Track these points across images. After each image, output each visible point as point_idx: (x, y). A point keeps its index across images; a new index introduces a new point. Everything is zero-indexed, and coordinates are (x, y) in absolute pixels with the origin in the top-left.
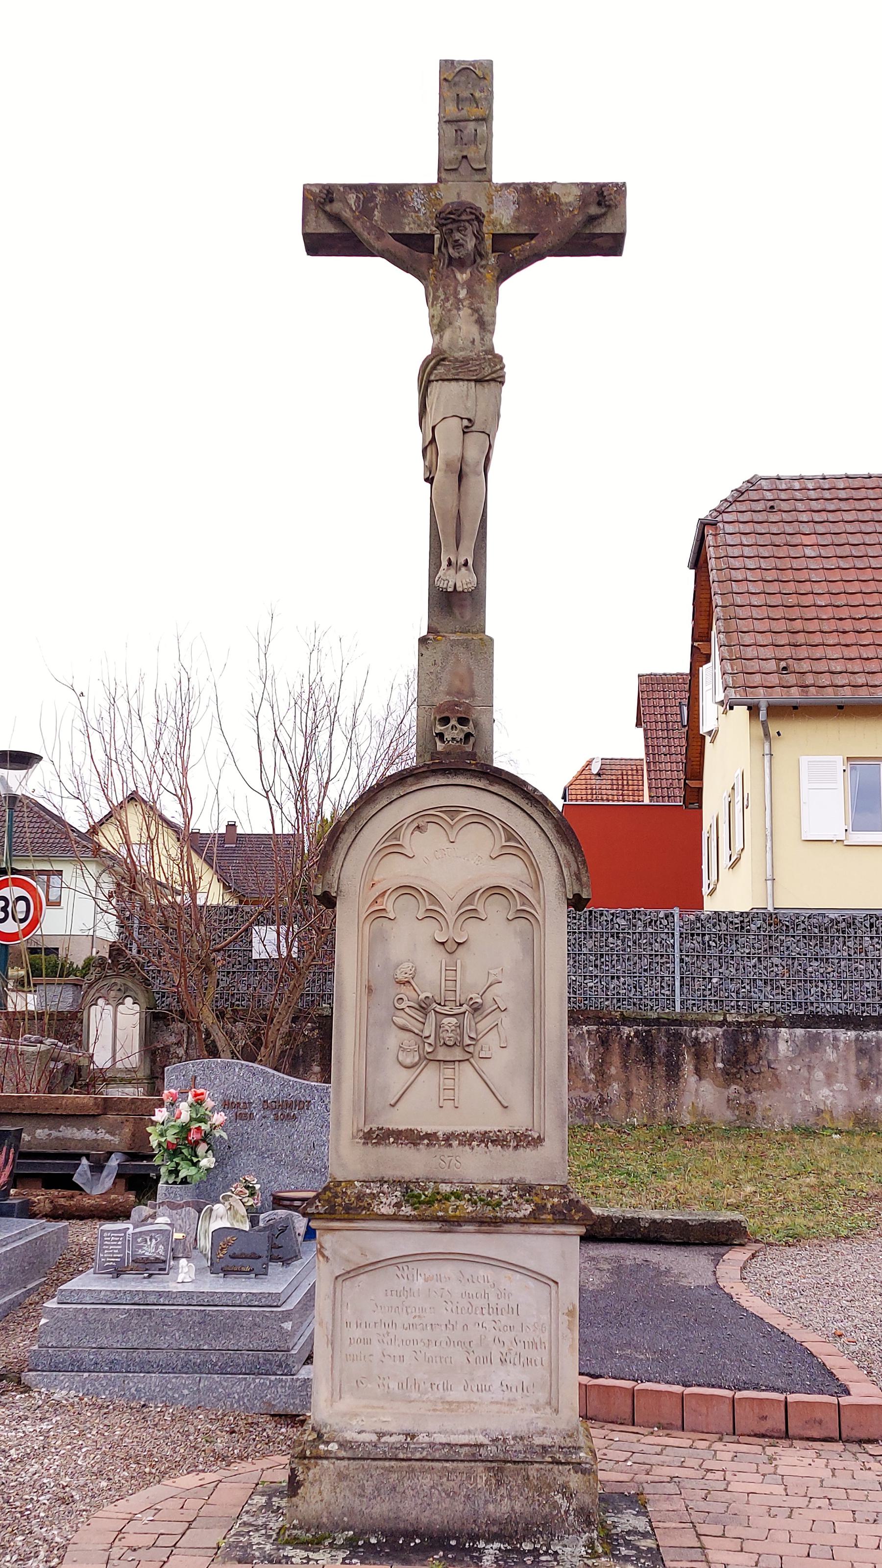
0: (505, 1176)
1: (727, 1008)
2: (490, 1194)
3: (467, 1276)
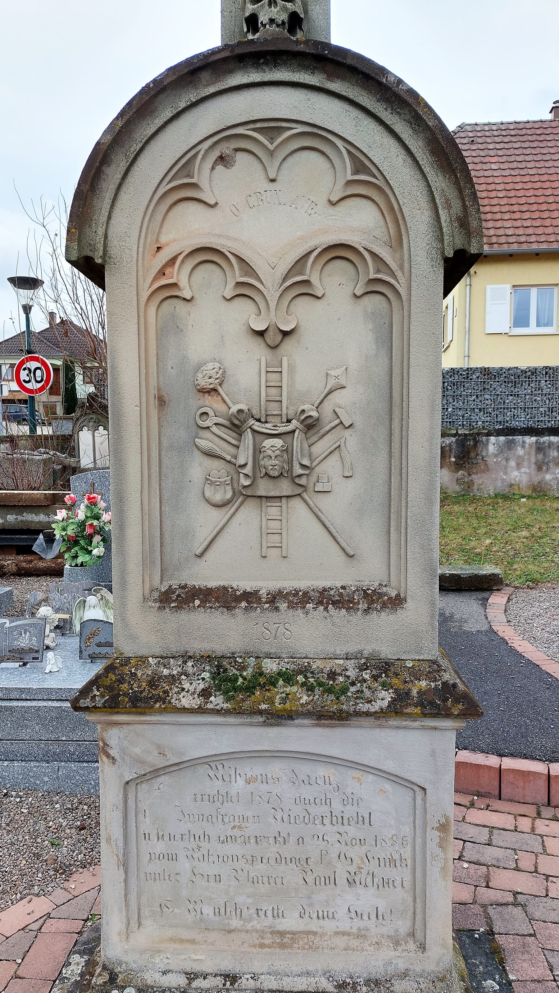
0: (352, 648)
1: (457, 426)
2: (332, 675)
3: (303, 777)
